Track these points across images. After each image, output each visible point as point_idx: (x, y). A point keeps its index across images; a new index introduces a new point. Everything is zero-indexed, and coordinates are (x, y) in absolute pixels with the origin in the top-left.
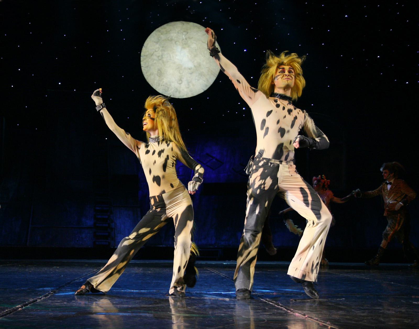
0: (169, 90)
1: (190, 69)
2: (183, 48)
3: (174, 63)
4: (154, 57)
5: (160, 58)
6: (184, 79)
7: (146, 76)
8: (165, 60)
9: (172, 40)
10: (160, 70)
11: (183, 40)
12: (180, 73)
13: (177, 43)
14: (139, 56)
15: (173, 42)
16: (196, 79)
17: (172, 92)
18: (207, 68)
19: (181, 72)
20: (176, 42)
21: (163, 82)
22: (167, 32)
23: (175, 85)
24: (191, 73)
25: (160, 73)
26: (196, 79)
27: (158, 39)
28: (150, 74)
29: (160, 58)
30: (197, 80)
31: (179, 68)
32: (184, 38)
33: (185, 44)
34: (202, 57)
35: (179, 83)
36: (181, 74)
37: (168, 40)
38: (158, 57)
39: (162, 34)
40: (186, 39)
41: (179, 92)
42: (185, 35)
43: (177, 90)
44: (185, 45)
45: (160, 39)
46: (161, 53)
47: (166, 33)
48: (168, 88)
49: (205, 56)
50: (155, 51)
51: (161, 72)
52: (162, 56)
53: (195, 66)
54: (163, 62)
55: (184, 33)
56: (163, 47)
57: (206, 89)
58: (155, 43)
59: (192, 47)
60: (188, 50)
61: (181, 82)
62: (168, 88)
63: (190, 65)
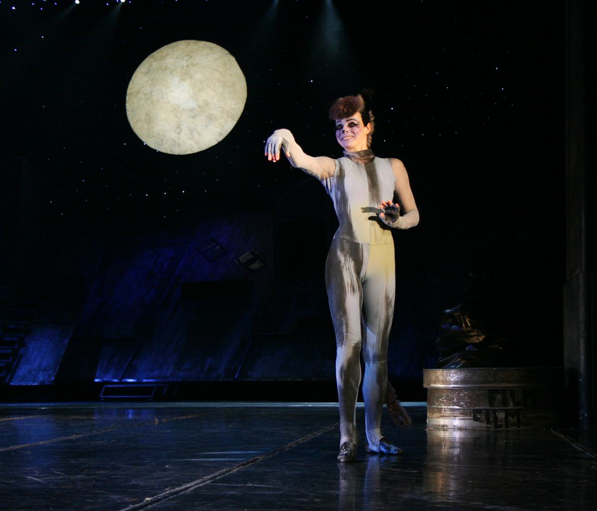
0: (164, 142)
1: (191, 111)
2: (183, 80)
3: (168, 103)
4: (141, 95)
5: (148, 96)
6: (184, 127)
7: (132, 125)
8: (154, 98)
9: (166, 68)
10: (148, 114)
11: (183, 67)
12: (176, 116)
13: (174, 72)
14: (220, 144)
15: (168, 72)
16: (202, 125)
17: (168, 146)
18: (219, 107)
19: (178, 115)
20: (171, 72)
21: (154, 131)
22: (163, 58)
23: (189, 142)
24: (194, 117)
25: (149, 119)
26: (202, 125)
27: (149, 69)
28: (137, 121)
29: (148, 96)
30: (204, 127)
31: (175, 110)
32: (185, 65)
33: (185, 74)
34: (211, 92)
35: (177, 131)
36: (178, 118)
37: (161, 69)
38: (146, 94)
39: (155, 61)
40: (187, 66)
41: (179, 145)
42: (186, 61)
43: (175, 143)
44: (186, 75)
45: (151, 68)
46: (149, 89)
47: (161, 59)
48: (162, 140)
49: (215, 91)
50: (143, 87)
51: (150, 117)
52: (151, 93)
53: (199, 106)
54: (206, 126)
55: (186, 58)
56: (153, 80)
57: (220, 139)
58: (143, 75)
59: (196, 77)
60: (189, 83)
61: (179, 130)
62: (162, 140)
63: (192, 104)
